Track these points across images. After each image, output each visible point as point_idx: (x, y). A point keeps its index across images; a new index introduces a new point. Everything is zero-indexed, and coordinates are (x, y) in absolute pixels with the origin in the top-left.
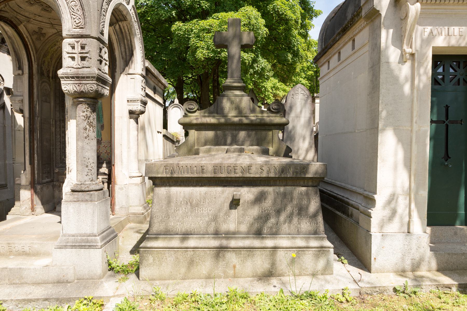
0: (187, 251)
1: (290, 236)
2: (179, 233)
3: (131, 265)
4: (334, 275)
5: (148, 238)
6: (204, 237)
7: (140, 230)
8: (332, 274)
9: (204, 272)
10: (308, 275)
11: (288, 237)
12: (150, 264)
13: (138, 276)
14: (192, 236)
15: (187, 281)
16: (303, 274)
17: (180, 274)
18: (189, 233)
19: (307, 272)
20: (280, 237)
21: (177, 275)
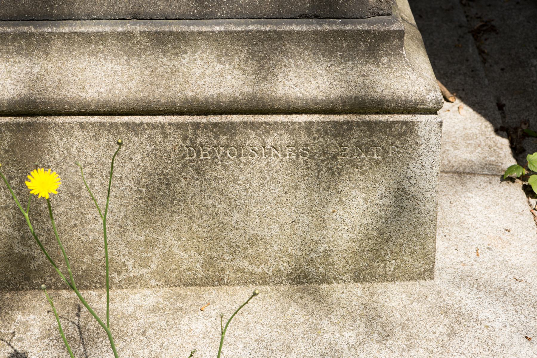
1: (138, 27)
4: (440, 281)
8: (428, 274)
10: (264, 280)
11: (127, 36)
16: (229, 274)
19: (256, 259)
20: (69, 38)
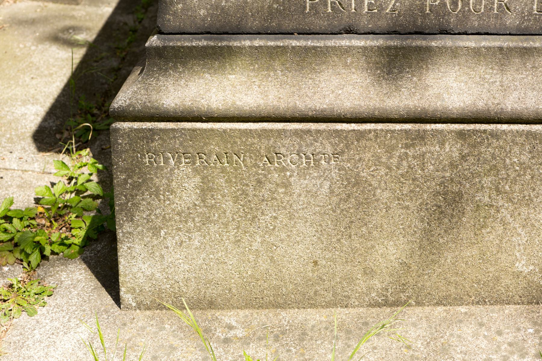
0: (421, 137)
2: (365, 23)
3: (59, 213)
5: (160, 53)
6: (526, 53)
7: (67, 29)
9: (521, 266)
12: (184, 216)
13: (108, 276)
14: (448, 41)
15: (415, 313)
17: (368, 272)
18: (432, 21)
21: (350, 279)
